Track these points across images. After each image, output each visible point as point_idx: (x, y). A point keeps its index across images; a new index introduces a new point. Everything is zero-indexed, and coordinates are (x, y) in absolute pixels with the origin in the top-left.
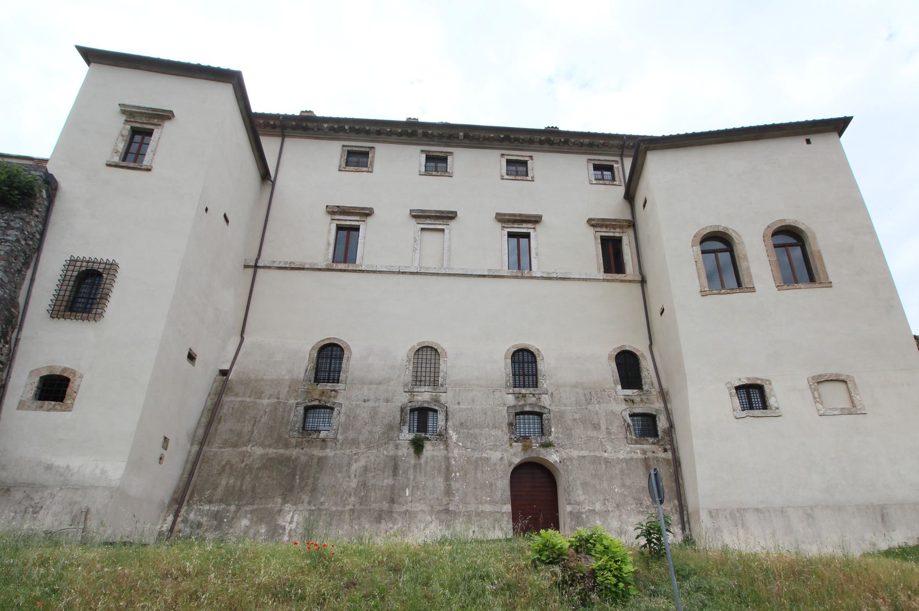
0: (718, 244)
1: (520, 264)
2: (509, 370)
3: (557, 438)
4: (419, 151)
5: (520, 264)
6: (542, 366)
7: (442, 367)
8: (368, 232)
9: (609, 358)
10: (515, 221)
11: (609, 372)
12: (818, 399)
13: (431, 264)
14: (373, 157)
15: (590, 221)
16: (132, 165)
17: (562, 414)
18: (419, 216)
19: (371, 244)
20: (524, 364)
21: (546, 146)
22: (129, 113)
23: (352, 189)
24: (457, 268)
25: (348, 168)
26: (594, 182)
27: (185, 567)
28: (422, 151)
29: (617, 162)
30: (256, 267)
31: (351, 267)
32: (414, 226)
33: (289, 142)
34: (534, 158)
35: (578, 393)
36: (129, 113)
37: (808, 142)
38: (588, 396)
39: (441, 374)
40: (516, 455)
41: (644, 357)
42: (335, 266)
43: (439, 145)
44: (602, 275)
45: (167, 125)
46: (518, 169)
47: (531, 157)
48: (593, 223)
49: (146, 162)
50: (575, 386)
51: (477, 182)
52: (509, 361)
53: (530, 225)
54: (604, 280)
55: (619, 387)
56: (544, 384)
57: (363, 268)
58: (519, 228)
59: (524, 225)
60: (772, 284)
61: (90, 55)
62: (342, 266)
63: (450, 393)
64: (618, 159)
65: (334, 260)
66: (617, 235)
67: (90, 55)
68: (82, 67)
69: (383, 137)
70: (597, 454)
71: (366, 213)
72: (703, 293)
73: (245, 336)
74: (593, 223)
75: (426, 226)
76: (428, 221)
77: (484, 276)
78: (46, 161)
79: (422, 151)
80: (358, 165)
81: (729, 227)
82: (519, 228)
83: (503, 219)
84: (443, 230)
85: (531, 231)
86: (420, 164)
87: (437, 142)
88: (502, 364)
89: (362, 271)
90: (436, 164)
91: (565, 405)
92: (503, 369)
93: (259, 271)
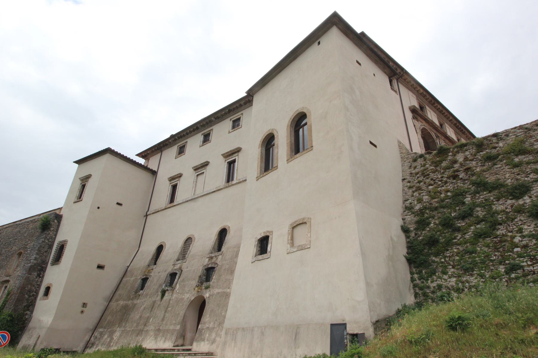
12: (302, 248)
30: (147, 216)
43: (208, 128)
59: (234, 155)
61: (76, 162)
67: (76, 162)
68: (77, 165)
69: (231, 112)
70: (225, 290)
78: (60, 209)
84: (203, 173)
93: (148, 217)
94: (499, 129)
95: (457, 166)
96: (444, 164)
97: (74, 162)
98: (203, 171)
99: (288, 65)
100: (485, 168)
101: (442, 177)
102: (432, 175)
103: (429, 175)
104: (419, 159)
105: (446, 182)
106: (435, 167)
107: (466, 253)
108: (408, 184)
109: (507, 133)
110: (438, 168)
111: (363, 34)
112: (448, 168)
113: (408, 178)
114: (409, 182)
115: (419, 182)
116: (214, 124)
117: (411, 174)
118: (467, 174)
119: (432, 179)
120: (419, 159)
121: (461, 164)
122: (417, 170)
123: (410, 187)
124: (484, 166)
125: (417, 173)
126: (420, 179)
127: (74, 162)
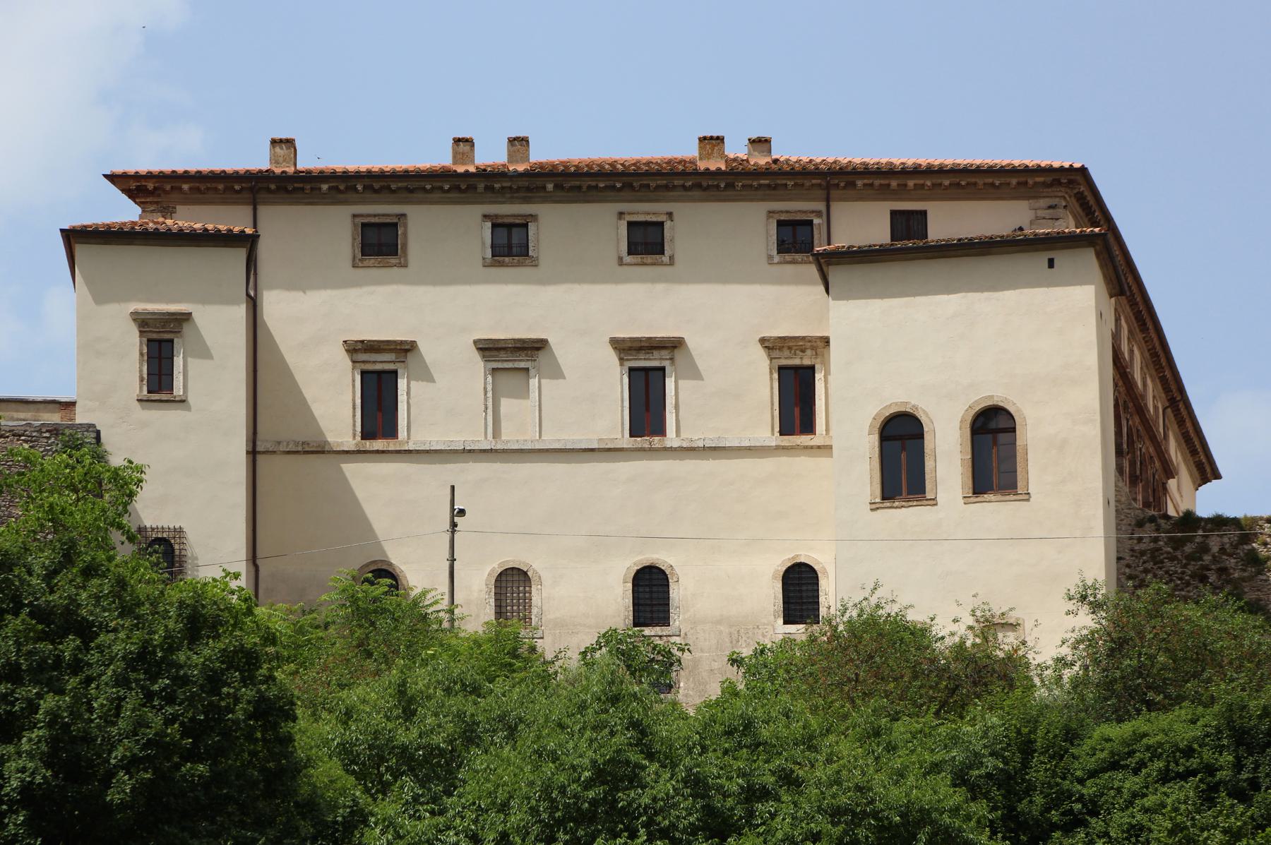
0: (901, 437)
1: (647, 410)
3: (686, 696)
4: (479, 218)
5: (647, 410)
6: (676, 593)
9: (774, 577)
11: (773, 594)
13: (512, 436)
14: (405, 234)
16: (164, 397)
18: (488, 349)
19: (425, 411)
21: (697, 193)
23: (380, 306)
24: (552, 439)
25: (371, 261)
26: (777, 259)
28: (486, 217)
31: (391, 445)
33: (263, 211)
34: (675, 216)
35: (721, 632)
37: (1051, 264)
38: (735, 636)
39: (535, 611)
40: (896, 725)
41: (825, 572)
44: (774, 439)
47: (670, 215)
49: (178, 390)
50: (719, 622)
52: (630, 585)
53: (665, 353)
54: (777, 448)
55: (781, 621)
56: (678, 619)
57: (411, 447)
58: (648, 379)
59: (656, 354)
62: (379, 444)
64: (821, 206)
65: (365, 436)
66: (807, 362)
73: (258, 562)
75: (500, 365)
76: (503, 355)
77: (592, 450)
79: (486, 217)
80: (379, 253)
81: (921, 405)
82: (648, 379)
83: (624, 348)
84: (527, 370)
85: (666, 364)
86: (483, 243)
87: (511, 204)
89: (410, 452)
91: (702, 651)
92: (619, 599)
95: (1207, 558)
96: (1188, 548)
97: (112, 178)
98: (522, 365)
99: (725, 201)
100: (1246, 574)
101: (1183, 573)
102: (1168, 563)
103: (1162, 562)
104: (1148, 525)
105: (1188, 584)
106: (1175, 549)
107: (1000, 678)
108: (1127, 570)
110: (1178, 554)
111: (186, 172)
112: (1190, 558)
113: (1127, 556)
114: (1128, 566)
115: (1146, 571)
117: (1132, 550)
118: (1219, 578)
119: (1167, 572)
120: (1148, 525)
121: (1214, 556)
122: (1143, 546)
123: (1130, 577)
124: (1244, 570)
125: (1143, 553)
126: (1150, 565)
127: (112, 178)
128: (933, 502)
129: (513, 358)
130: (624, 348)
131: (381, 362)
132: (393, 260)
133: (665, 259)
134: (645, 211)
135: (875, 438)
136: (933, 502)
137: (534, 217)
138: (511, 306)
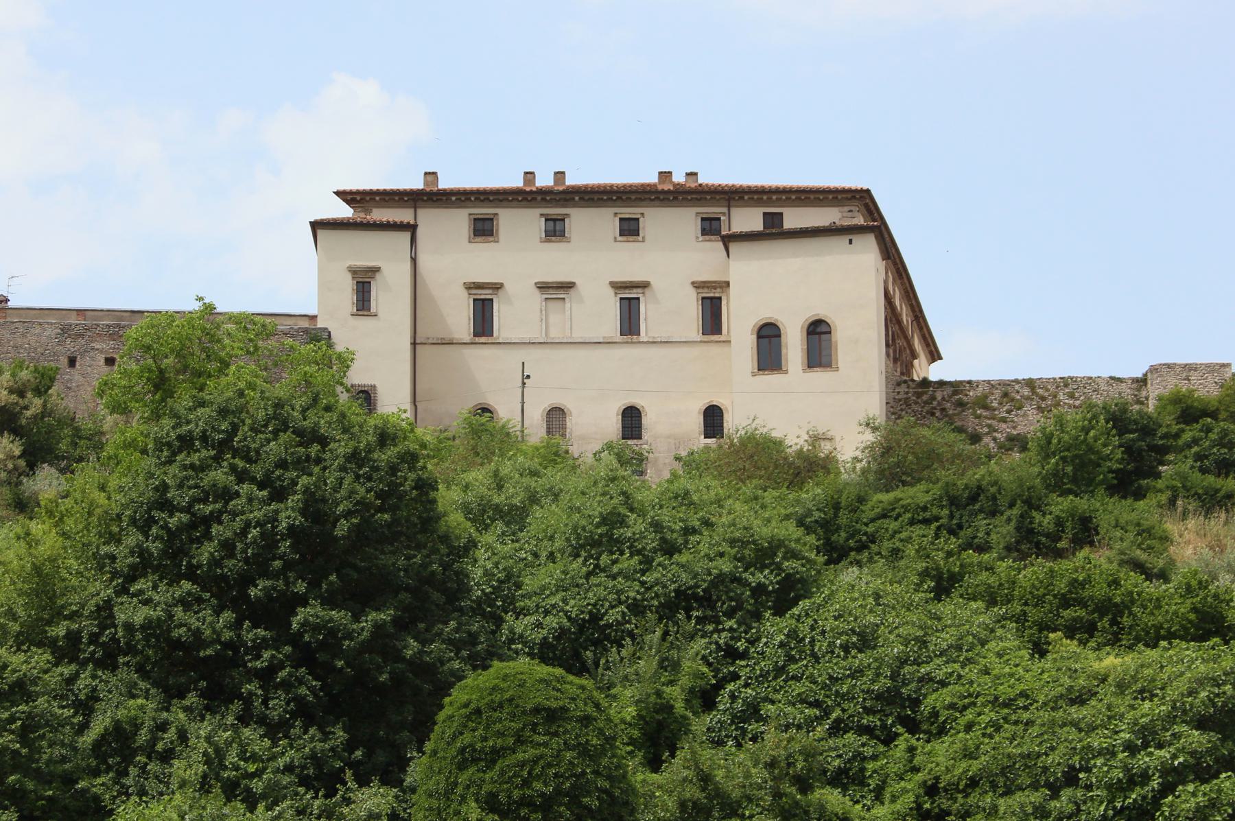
0: (768, 335)
1: (630, 323)
2: (620, 425)
5: (630, 323)
6: (645, 421)
7: (568, 424)
8: (500, 312)
10: (626, 288)
11: (697, 422)
13: (555, 334)
15: (693, 283)
17: (656, 459)
18: (543, 287)
19: (504, 319)
20: (632, 419)
21: (657, 203)
22: (354, 272)
23: (483, 262)
24: (578, 336)
27: (185, 611)
28: (542, 215)
29: (724, 214)
31: (490, 340)
32: (537, 297)
36: (354, 272)
42: (477, 340)
44: (700, 337)
45: (378, 276)
46: (630, 229)
48: (698, 286)
50: (669, 437)
51: (594, 256)
53: (640, 290)
56: (646, 435)
58: (630, 304)
59: (635, 290)
60: (800, 368)
62: (483, 339)
63: (575, 446)
64: (725, 210)
65: (475, 335)
71: (497, 287)
72: (754, 375)
74: (698, 286)
76: (551, 291)
79: (542, 215)
82: (630, 304)
87: (556, 204)
88: (614, 420)
90: (555, 231)
94: (974, 379)
109: (978, 383)
116: (574, 206)
128: (786, 372)
129: (556, 290)
130: (618, 286)
131: (484, 294)
132: (491, 239)
133: (640, 238)
134: (628, 212)
135: (754, 337)
136: (786, 372)
137: (568, 215)
138: (556, 262)
